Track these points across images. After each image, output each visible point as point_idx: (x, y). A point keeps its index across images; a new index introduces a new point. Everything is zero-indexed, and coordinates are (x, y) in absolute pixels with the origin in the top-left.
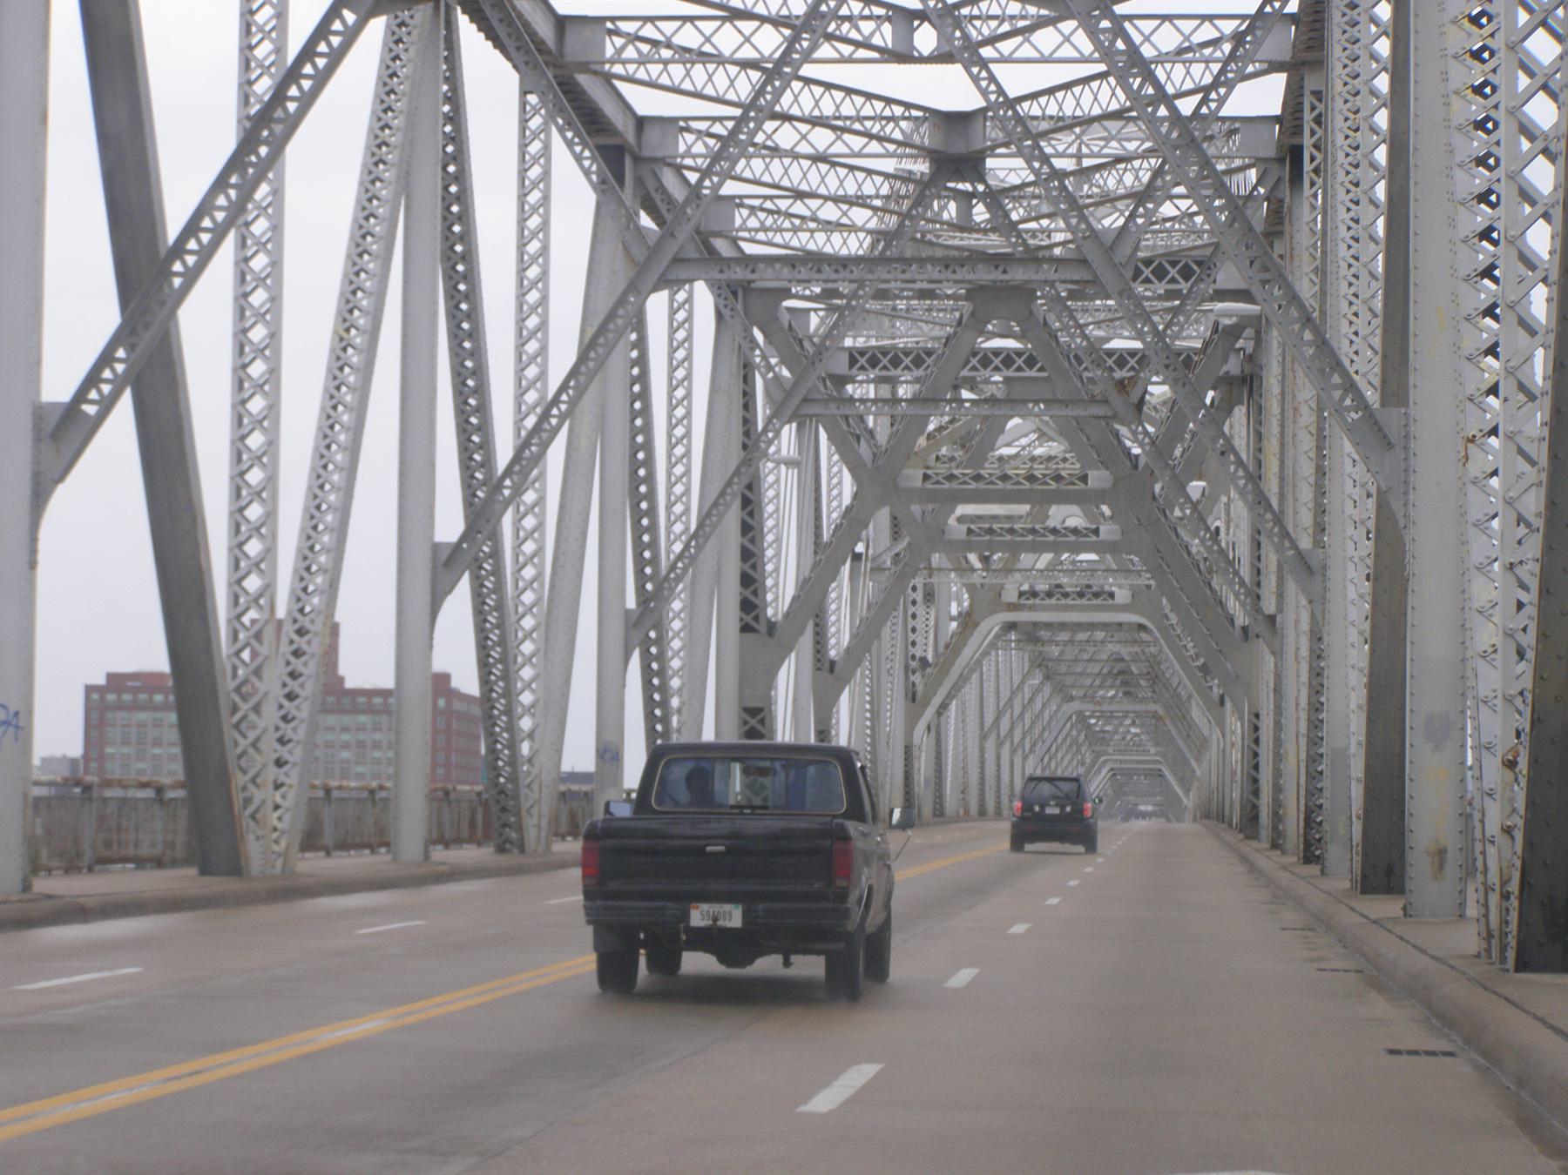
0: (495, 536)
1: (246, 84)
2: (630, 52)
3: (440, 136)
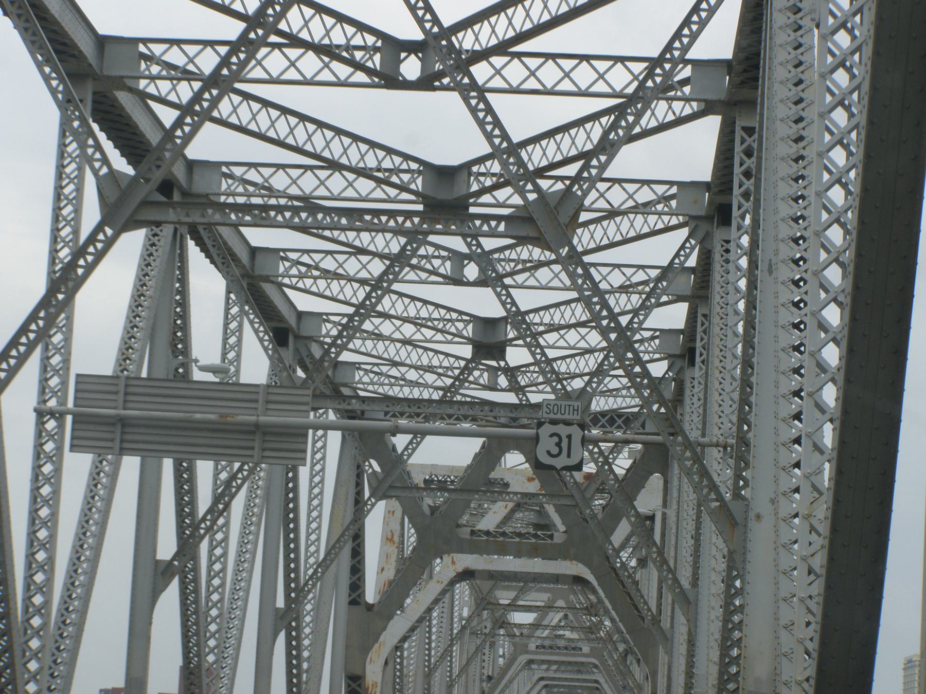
0: (195, 558)
1: (53, 252)
2: (294, 271)
3: (174, 302)
